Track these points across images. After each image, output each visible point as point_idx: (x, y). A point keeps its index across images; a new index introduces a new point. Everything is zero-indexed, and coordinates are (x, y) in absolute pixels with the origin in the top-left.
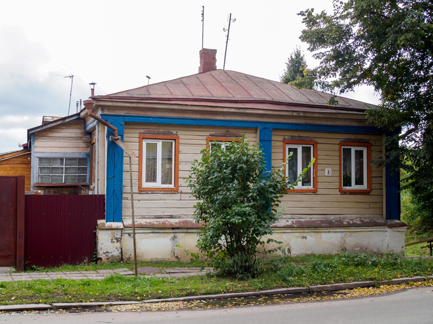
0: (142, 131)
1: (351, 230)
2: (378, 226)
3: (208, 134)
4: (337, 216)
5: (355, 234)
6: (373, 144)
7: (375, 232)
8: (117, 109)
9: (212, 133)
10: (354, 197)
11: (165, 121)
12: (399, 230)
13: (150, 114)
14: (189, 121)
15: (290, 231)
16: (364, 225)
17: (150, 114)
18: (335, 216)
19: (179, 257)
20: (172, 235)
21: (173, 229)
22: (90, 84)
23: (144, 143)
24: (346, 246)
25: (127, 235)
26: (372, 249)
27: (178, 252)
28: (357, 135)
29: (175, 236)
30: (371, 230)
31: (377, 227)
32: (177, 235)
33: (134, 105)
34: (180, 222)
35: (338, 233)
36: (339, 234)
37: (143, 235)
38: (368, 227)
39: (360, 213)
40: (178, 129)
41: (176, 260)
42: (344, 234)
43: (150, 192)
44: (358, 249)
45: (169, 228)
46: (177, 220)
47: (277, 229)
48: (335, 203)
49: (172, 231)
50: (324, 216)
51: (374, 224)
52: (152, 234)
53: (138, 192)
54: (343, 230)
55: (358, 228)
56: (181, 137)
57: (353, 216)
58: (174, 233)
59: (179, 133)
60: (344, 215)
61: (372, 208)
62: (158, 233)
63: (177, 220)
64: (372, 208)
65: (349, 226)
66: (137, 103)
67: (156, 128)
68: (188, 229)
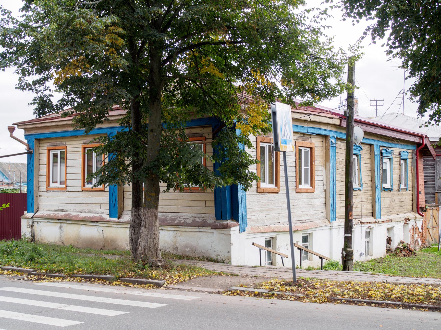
0: (48, 144)
1: (180, 229)
2: (204, 226)
3: (82, 142)
4: (175, 214)
5: (184, 233)
6: (207, 138)
7: (204, 233)
8: (32, 130)
9: (85, 141)
10: (190, 195)
11: (54, 135)
12: (223, 232)
13: (47, 131)
14: (67, 133)
15: (115, 226)
16: (195, 224)
17: (47, 131)
18: (173, 214)
19: (64, 242)
20: (59, 225)
21: (59, 220)
22: (324, 29)
23: (52, 153)
24: (177, 245)
25: (36, 223)
26: (201, 250)
27: (63, 239)
28: (191, 129)
29: (61, 226)
30: (198, 230)
31: (203, 228)
32: (62, 225)
33: (34, 126)
34: (65, 215)
35: (170, 232)
36: (171, 233)
37: (44, 224)
38: (194, 227)
39: (196, 212)
40: (66, 140)
41: (62, 245)
42: (175, 232)
43: (52, 191)
44: (189, 249)
45: (56, 219)
46: (63, 213)
47: (120, 224)
48: (174, 201)
49: (58, 221)
50: (164, 213)
51: (204, 224)
52: (49, 223)
53: (46, 191)
54: (173, 229)
55: (186, 227)
56: (68, 146)
57: (189, 214)
58: (60, 223)
59: (67, 143)
60: (182, 214)
61: (209, 207)
62: (73, 224)
63: (63, 213)
64: (209, 207)
65: (185, 225)
66: (33, 124)
67: (55, 141)
68: (66, 220)
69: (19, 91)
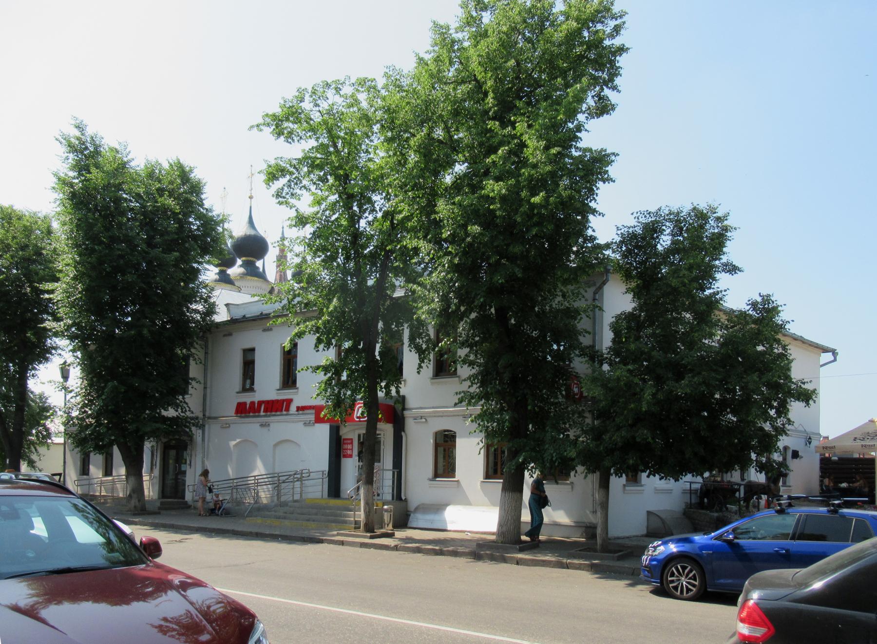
22: (619, 91)
69: (616, 152)
